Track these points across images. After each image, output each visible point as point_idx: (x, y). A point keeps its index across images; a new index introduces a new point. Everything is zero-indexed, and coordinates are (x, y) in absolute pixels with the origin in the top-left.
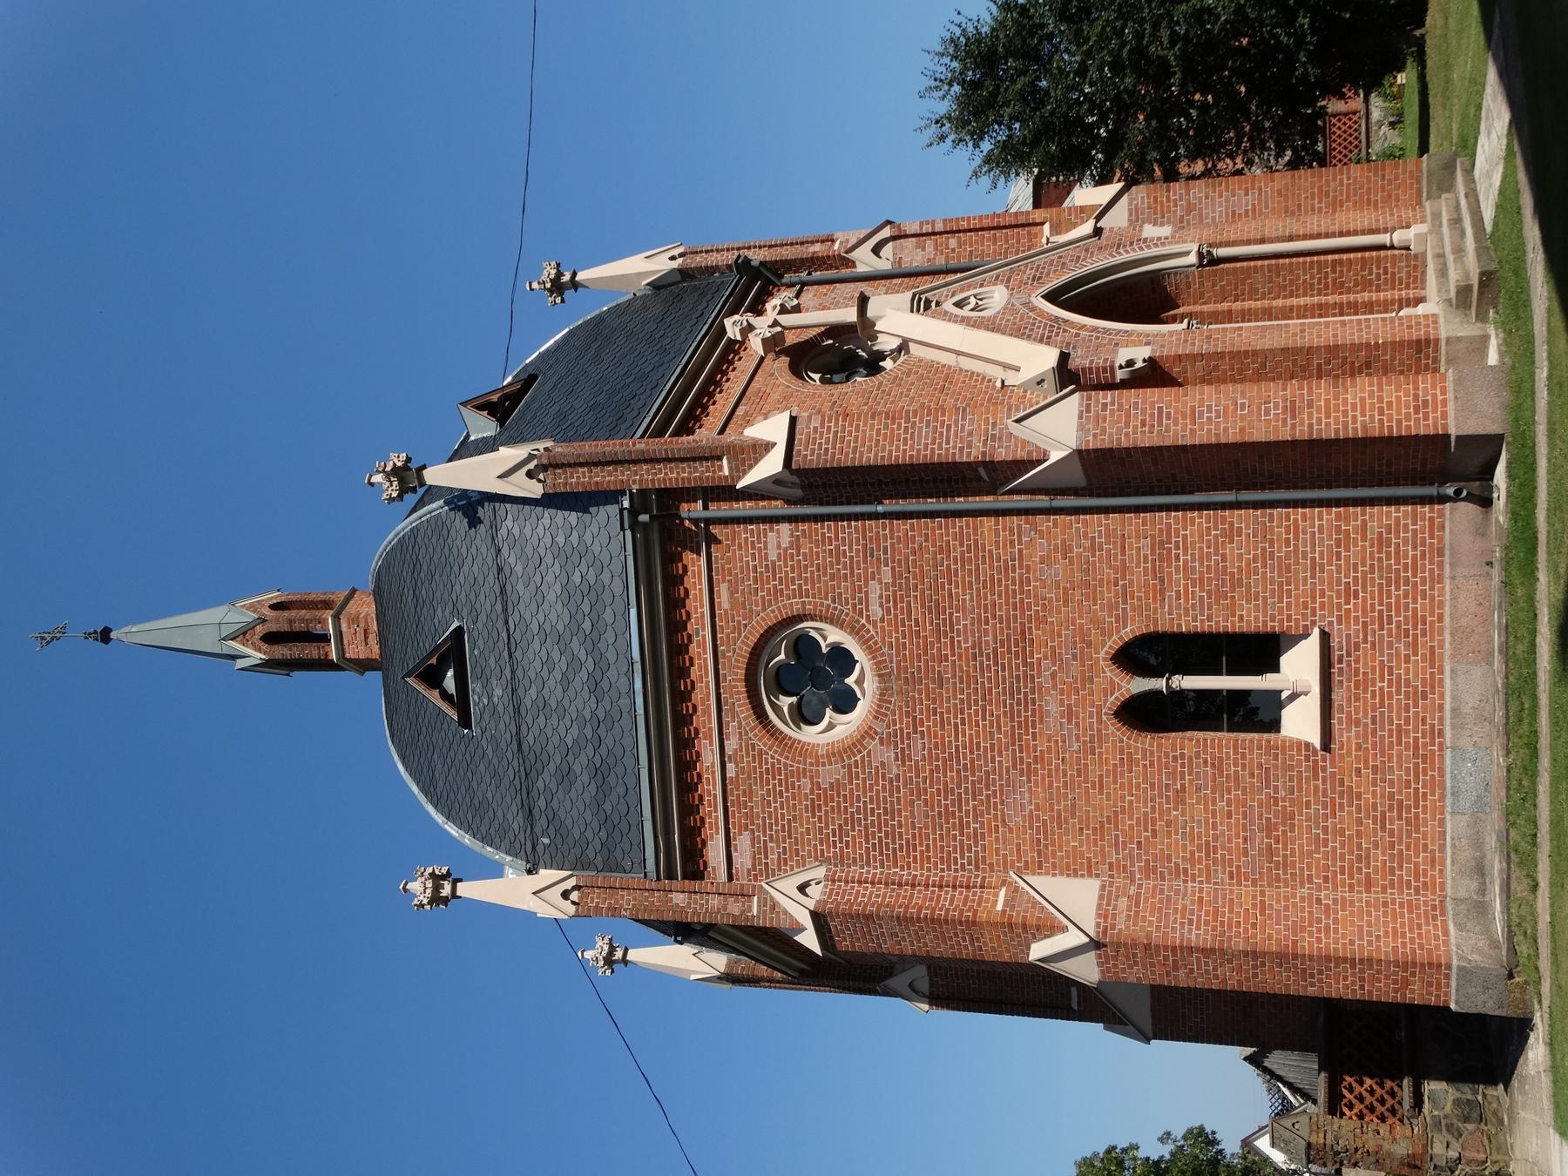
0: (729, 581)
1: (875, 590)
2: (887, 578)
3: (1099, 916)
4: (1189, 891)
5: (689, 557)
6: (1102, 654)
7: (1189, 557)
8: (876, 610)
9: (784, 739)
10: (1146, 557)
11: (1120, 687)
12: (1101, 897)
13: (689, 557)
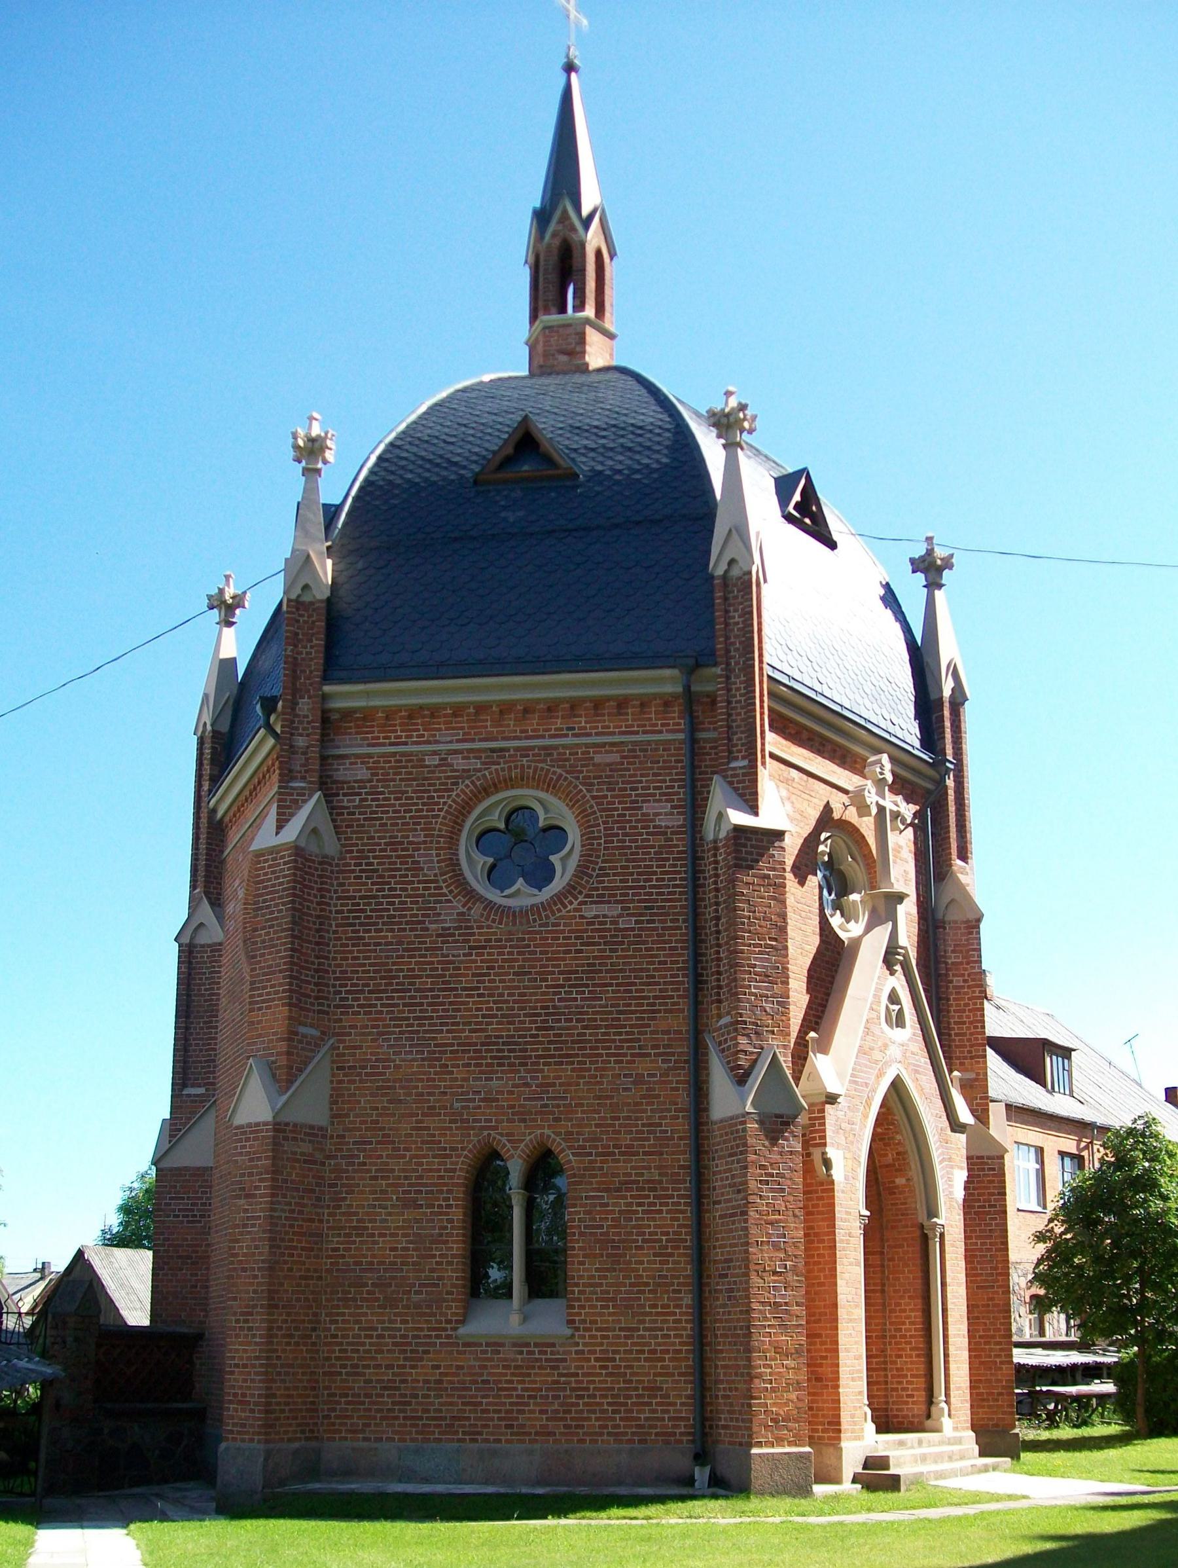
3: (295, 1125)
8: (591, 911)
12: (312, 1127)
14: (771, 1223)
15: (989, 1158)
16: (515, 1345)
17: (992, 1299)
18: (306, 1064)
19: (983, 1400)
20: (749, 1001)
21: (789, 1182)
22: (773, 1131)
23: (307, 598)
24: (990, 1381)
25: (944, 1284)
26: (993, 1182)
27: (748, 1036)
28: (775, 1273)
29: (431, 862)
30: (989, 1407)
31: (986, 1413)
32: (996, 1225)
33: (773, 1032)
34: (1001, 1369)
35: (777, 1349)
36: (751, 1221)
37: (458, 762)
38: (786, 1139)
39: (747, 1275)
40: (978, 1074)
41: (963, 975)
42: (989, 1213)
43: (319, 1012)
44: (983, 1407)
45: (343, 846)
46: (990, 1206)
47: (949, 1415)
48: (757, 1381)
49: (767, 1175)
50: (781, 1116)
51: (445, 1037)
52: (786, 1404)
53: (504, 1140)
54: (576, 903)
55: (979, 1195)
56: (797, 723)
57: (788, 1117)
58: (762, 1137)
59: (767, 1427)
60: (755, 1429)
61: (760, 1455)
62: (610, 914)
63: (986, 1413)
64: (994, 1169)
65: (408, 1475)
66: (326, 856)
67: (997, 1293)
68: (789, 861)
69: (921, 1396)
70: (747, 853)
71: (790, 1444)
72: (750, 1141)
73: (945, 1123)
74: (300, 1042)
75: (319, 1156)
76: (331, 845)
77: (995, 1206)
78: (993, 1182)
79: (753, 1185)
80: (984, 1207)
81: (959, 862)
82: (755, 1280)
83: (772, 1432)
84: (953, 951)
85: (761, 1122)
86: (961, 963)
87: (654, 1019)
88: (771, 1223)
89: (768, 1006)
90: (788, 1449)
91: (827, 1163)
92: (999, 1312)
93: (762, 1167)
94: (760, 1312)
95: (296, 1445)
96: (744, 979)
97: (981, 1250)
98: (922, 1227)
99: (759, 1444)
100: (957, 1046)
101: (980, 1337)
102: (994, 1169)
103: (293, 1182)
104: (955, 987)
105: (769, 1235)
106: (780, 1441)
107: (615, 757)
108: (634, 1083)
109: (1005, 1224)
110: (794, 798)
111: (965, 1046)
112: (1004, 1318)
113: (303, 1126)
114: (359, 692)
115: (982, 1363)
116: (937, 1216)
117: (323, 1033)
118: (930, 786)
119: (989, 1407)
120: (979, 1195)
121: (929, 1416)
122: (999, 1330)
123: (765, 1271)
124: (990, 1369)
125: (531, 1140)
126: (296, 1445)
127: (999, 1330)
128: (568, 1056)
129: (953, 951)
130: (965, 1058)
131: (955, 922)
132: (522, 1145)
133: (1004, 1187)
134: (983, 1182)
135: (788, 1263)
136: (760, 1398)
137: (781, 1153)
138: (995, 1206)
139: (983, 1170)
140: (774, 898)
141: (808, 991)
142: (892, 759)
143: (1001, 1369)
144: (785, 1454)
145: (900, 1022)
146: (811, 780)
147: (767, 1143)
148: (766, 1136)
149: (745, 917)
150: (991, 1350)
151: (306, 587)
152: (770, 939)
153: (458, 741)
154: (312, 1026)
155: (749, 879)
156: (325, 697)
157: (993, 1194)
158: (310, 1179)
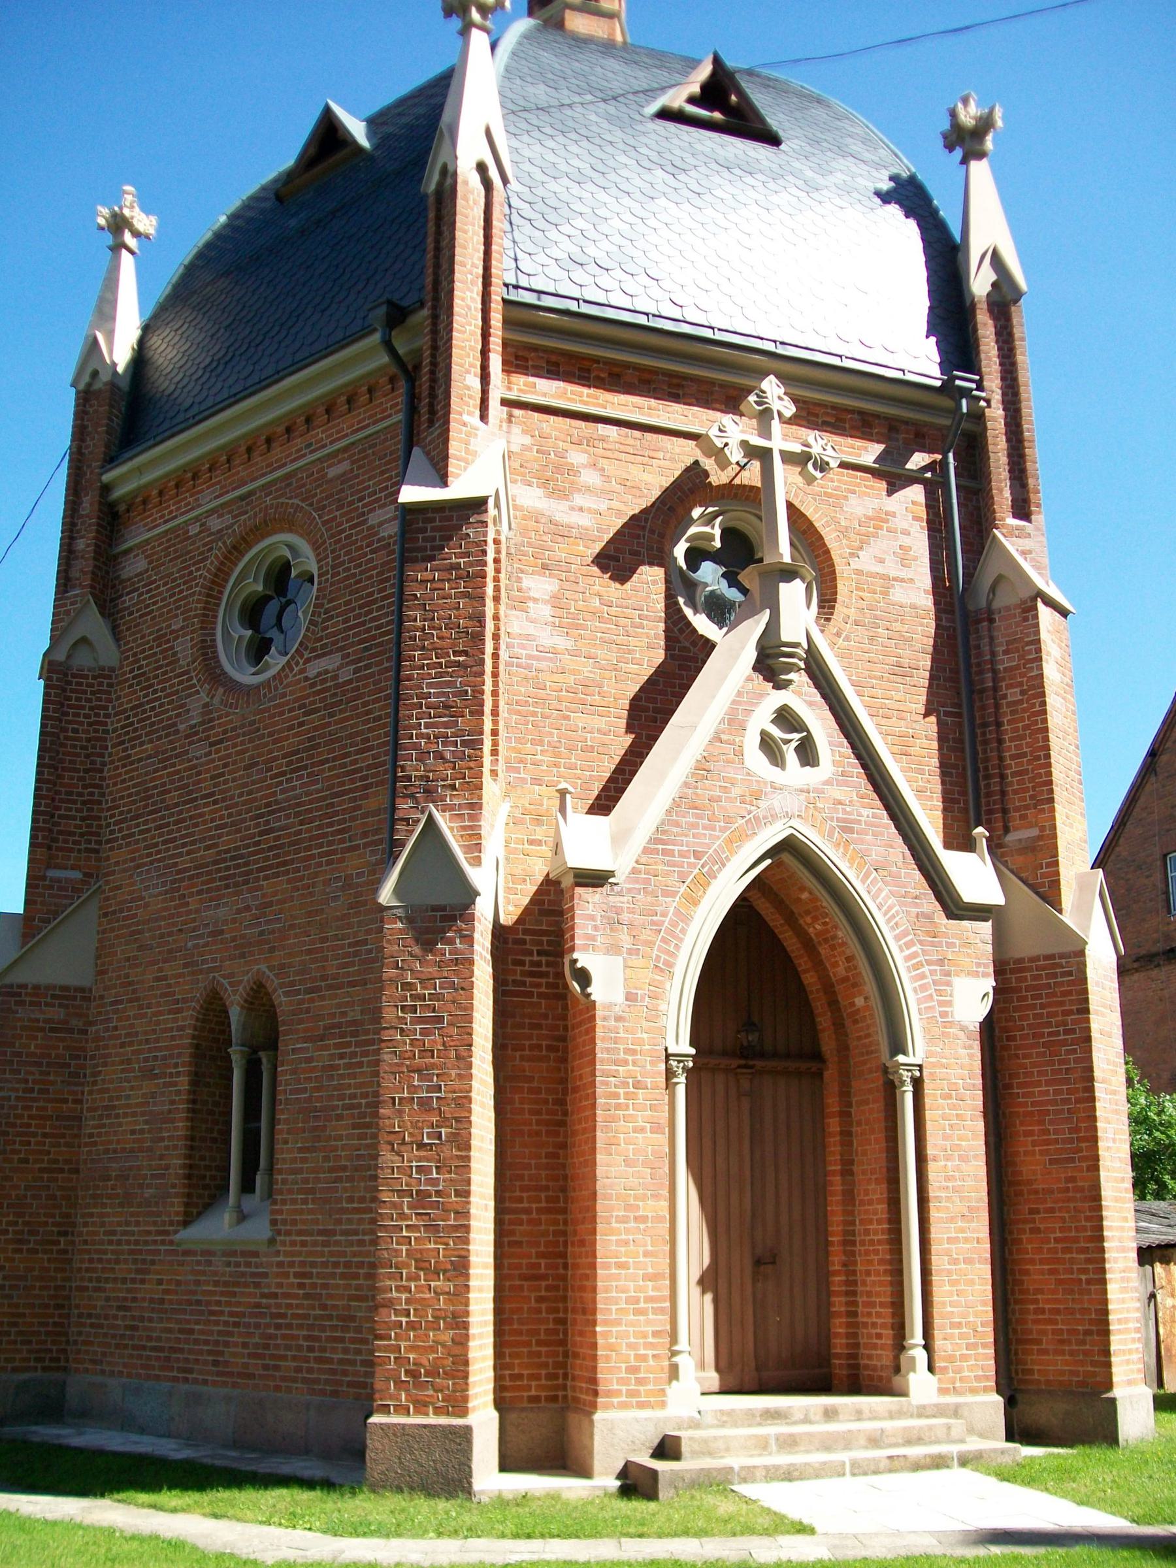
0: (352, 470)
1: (331, 663)
2: (345, 675)
3: (36, 987)
4: (75, 1088)
5: (878, 448)
6: (263, 967)
7: (1061, 1029)
8: (313, 670)
9: (219, 585)
10: (344, 1014)
11: (235, 992)
12: (65, 988)
13: (878, 448)
14: (418, 1071)
15: (1062, 956)
16: (225, 1254)
17: (1072, 1179)
18: (56, 914)
19: (1062, 1342)
20: (416, 747)
21: (452, 1007)
22: (427, 931)
23: (98, 386)
24: (1072, 1312)
25: (921, 1158)
26: (1070, 993)
27: (412, 796)
28: (421, 1146)
29: (185, 648)
30: (1072, 1353)
31: (1066, 1363)
32: (1076, 1061)
33: (453, 787)
34: (1089, 1292)
35: (421, 1263)
36: (384, 1067)
37: (215, 524)
38: (451, 942)
39: (375, 1146)
40: (1042, 829)
41: (1021, 684)
42: (1064, 1043)
43: (87, 850)
44: (1062, 1353)
45: (123, 653)
46: (1066, 1032)
47: (931, 1368)
48: (383, 1311)
49: (414, 997)
50: (443, 908)
51: (184, 862)
52: (433, 1349)
53: (225, 982)
54: (301, 662)
55: (1049, 1015)
56: (636, 368)
57: (453, 908)
58: (410, 941)
59: (399, 1383)
60: (378, 1385)
61: (381, 1426)
62: (330, 667)
63: (1066, 1363)
64: (1070, 974)
65: (127, 1423)
66: (103, 669)
67: (1080, 1170)
68: (684, 567)
69: (888, 1339)
70: (425, 540)
71: (438, 1411)
72: (389, 949)
73: (931, 904)
74: (51, 887)
75: (75, 1022)
76: (107, 653)
77: (1073, 1031)
78: (1070, 993)
79: (390, 1014)
80: (1057, 1033)
81: (1012, 521)
82: (387, 1158)
83: (407, 1391)
84: (1006, 652)
85: (409, 920)
86: (1017, 667)
87: (366, 797)
88: (418, 1071)
89: (448, 752)
90: (432, 1420)
91: (584, 977)
92: (1084, 1199)
93: (407, 986)
94: (394, 1205)
95: (25, 1376)
96: (410, 717)
97: (1054, 1102)
98: (885, 1070)
99: (385, 1410)
100: (1016, 792)
101: (1057, 1240)
102: (1070, 974)
103: (33, 1054)
104: (1009, 704)
105: (413, 1089)
106: (421, 1406)
107: (345, 466)
108: (343, 888)
109: (1090, 1059)
110: (602, 463)
111: (1026, 790)
112: (1092, 1209)
113: (49, 987)
114: (130, 471)
115: (1060, 1282)
116: (905, 1052)
117: (85, 875)
118: (948, 422)
119: (1072, 1353)
120: (1049, 1015)
121: (897, 1369)
122: (1084, 1229)
123: (404, 1143)
124: (1072, 1292)
125: (248, 981)
126: (25, 1376)
127: (1084, 1229)
128: (285, 863)
129: (1006, 652)
130: (1027, 807)
131: (1008, 608)
132: (241, 988)
133: (1087, 1000)
134: (1054, 995)
135: (443, 1130)
136: (390, 1338)
137: (440, 964)
138: (1073, 1031)
139: (1055, 976)
140: (465, 595)
141: (629, 729)
142: (782, 377)
143: (1089, 1292)
144: (425, 1426)
145: (807, 753)
146: (648, 436)
147: (416, 949)
148: (417, 941)
149: (416, 629)
150: (1072, 1261)
151: (95, 374)
152: (456, 653)
153: (216, 498)
154: (73, 868)
155: (428, 575)
156: (106, 489)
157: (1070, 1012)
158: (61, 1051)
